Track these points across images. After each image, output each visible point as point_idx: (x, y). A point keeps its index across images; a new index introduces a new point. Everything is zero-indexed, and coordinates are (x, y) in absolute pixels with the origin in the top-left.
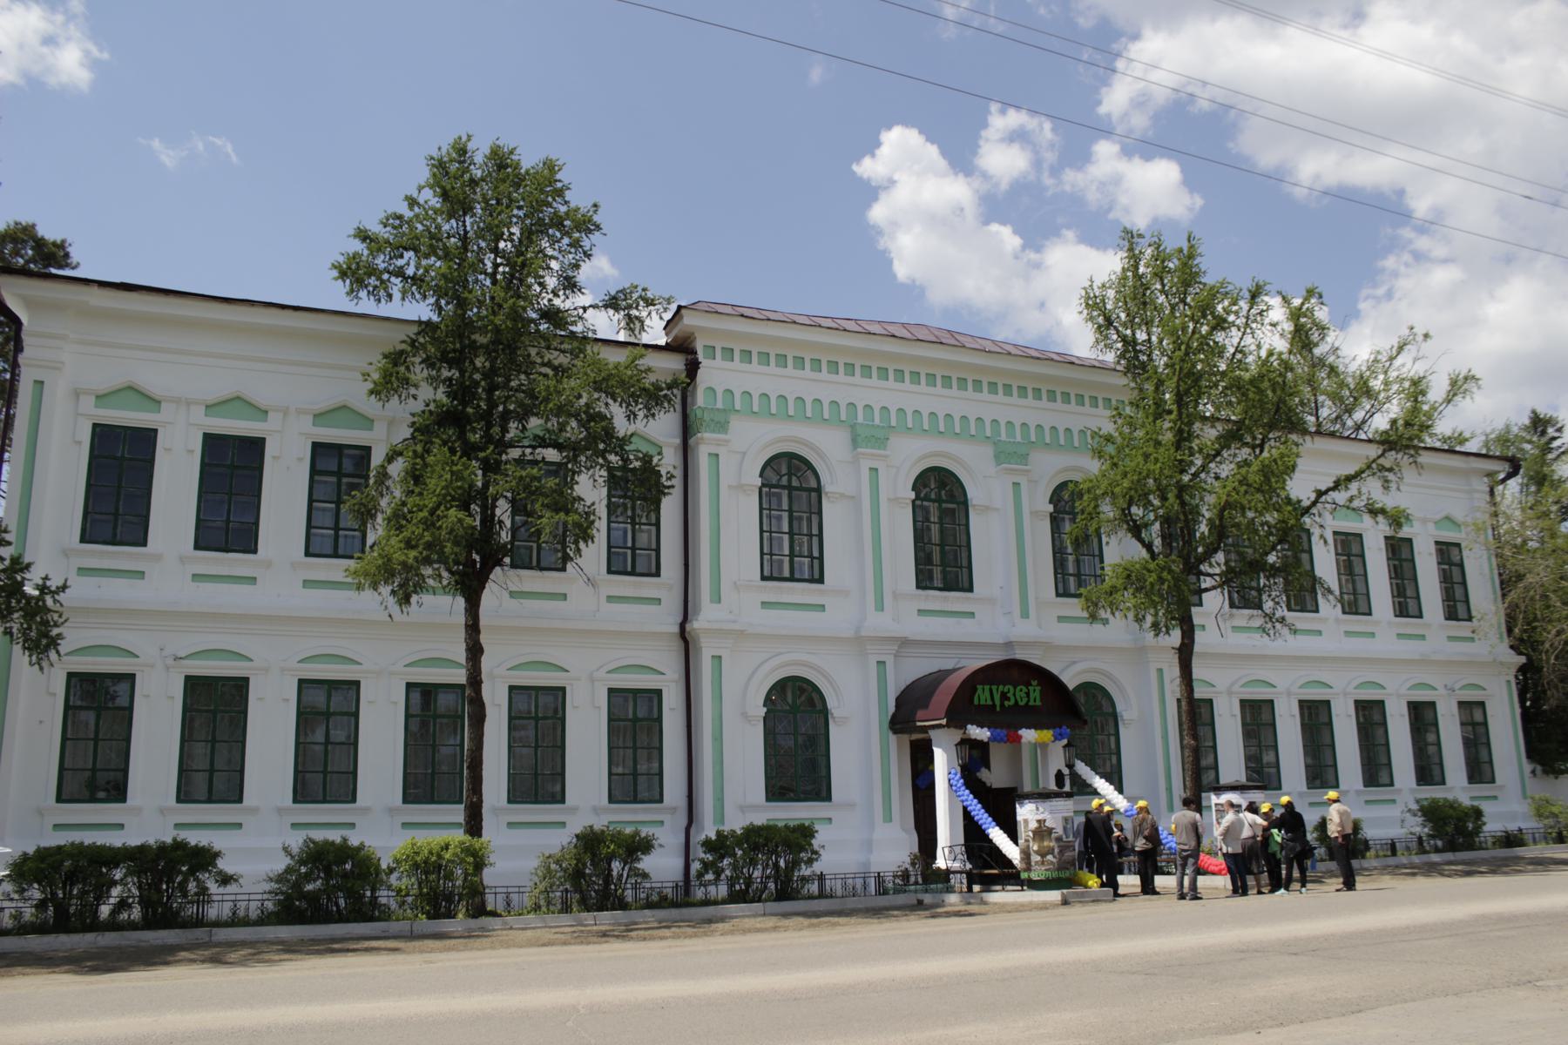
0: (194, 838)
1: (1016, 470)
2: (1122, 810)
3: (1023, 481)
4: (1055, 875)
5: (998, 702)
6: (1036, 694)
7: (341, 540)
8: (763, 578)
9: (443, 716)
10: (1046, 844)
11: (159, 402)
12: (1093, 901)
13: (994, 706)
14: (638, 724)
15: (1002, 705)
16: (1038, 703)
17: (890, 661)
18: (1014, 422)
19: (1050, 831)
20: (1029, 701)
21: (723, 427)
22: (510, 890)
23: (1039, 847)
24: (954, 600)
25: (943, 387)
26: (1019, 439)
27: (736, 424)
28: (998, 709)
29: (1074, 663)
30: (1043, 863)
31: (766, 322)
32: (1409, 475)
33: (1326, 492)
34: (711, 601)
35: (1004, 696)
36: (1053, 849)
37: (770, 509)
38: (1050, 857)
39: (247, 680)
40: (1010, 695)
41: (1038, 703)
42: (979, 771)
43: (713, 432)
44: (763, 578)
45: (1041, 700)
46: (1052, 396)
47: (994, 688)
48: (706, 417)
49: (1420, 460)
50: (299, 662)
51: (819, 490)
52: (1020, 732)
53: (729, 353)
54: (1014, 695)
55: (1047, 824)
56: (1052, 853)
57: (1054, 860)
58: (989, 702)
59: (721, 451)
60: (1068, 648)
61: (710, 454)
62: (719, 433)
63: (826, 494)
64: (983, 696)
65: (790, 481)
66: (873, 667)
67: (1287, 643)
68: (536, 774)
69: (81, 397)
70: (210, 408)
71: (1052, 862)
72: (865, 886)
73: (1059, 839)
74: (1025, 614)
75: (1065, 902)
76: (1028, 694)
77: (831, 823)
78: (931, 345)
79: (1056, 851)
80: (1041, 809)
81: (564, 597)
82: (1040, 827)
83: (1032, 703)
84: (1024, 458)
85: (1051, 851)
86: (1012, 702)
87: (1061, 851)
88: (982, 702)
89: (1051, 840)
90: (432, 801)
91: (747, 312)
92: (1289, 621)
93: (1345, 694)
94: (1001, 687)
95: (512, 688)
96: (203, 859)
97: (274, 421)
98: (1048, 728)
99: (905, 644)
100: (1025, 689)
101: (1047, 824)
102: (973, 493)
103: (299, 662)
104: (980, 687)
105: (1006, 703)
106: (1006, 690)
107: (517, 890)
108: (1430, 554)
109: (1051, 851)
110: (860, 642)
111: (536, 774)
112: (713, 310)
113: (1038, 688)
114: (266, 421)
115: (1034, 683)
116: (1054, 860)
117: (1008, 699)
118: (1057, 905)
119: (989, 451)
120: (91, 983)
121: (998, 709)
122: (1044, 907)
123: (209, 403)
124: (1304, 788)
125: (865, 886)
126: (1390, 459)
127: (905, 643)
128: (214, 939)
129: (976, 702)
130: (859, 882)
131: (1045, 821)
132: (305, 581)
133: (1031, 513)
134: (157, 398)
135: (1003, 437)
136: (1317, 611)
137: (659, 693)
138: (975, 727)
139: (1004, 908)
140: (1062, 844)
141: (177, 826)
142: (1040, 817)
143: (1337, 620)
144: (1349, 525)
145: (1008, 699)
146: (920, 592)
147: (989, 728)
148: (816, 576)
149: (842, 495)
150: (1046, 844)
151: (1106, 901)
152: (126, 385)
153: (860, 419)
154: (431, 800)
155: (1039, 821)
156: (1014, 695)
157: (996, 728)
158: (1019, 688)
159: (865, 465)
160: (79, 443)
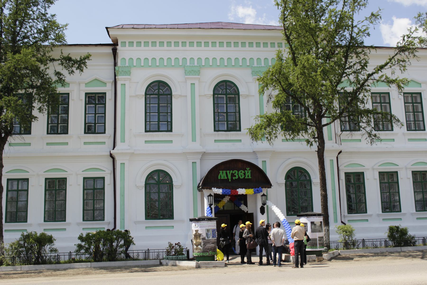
0: (49, 233)
1: (192, 78)
2: (111, 230)
3: (196, 82)
4: (201, 254)
5: (230, 177)
6: (248, 174)
7: (416, 124)
8: (146, 131)
9: (389, 181)
10: (198, 241)
11: (420, 84)
12: (214, 267)
13: (228, 179)
14: (95, 191)
15: (232, 179)
16: (250, 177)
17: (198, 162)
18: (224, 58)
19: (200, 235)
20: (245, 176)
21: (128, 73)
22: (139, 251)
23: (196, 242)
24: (232, 135)
25: (197, 46)
26: (263, 65)
27: (134, 72)
28: (230, 181)
29: (289, 159)
30: (197, 249)
31: (143, 29)
32: (413, 61)
33: (373, 74)
34: (121, 142)
35: (233, 175)
36: (201, 243)
37: (150, 104)
38: (199, 247)
39: (66, 178)
40: (236, 174)
41: (250, 177)
42: (240, 206)
43: (123, 75)
44: (146, 131)
45: (251, 176)
46: (258, 45)
47: (228, 172)
48: (120, 70)
49: (416, 54)
50: (6, 173)
51: (171, 94)
52: (237, 190)
53: (131, 44)
54: (238, 174)
55: (198, 232)
56: (200, 245)
57: (201, 248)
58: (226, 178)
59: (127, 83)
60: (285, 153)
61: (122, 84)
62: (126, 75)
63: (173, 95)
64: (222, 175)
65: (226, 91)
66: (191, 164)
67: (378, 146)
68: (55, 211)
69: (81, 85)
70: (87, 84)
71: (200, 249)
72: (381, 245)
73: (204, 239)
74: (194, 140)
75: (198, 267)
76: (245, 174)
77: (368, 221)
78: (159, 29)
79: (202, 244)
80: (197, 226)
81: (67, 144)
82: (196, 233)
83: (247, 177)
84: (198, 73)
85: (200, 244)
86: (237, 177)
87: (204, 244)
88: (222, 178)
89: (200, 239)
90: (16, 222)
91: (135, 27)
92: (378, 135)
93: (406, 169)
94: (231, 172)
95: (84, 178)
96: (50, 240)
97: (424, 87)
98: (252, 188)
99: (204, 155)
100: (243, 172)
101: (198, 232)
102: (242, 91)
103: (6, 173)
104: (221, 172)
105: (234, 178)
106: (234, 172)
107: (63, 254)
108: (73, 100)
109: (200, 244)
110: (185, 155)
111: (55, 211)
112: (122, 27)
113: (250, 171)
114: (69, 87)
115: (248, 169)
116: (201, 248)
117: (235, 176)
118: (193, 268)
119: (249, 71)
120: (141, 276)
121: (230, 181)
122: (191, 268)
123: (86, 83)
124: (414, 211)
125: (381, 245)
126: (403, 56)
127: (204, 154)
128: (402, 250)
129: (219, 178)
130: (378, 243)
131: (198, 231)
132: (215, 140)
133: (199, 96)
134: (420, 83)
135: (255, 65)
136: (392, 130)
137: (103, 178)
138: (215, 188)
139: (184, 269)
140: (205, 241)
141: (45, 230)
142: (196, 229)
143: (404, 134)
144: (382, 88)
145: (235, 176)
146: (216, 133)
147: (223, 189)
148: (169, 129)
149: (180, 96)
150: (198, 241)
151: (220, 267)
152: (94, 79)
153: (188, 64)
154: (16, 221)
155: (196, 231)
156: (238, 174)
157: (255, 188)
158: (240, 172)
159: (189, 82)
160: (82, 100)
